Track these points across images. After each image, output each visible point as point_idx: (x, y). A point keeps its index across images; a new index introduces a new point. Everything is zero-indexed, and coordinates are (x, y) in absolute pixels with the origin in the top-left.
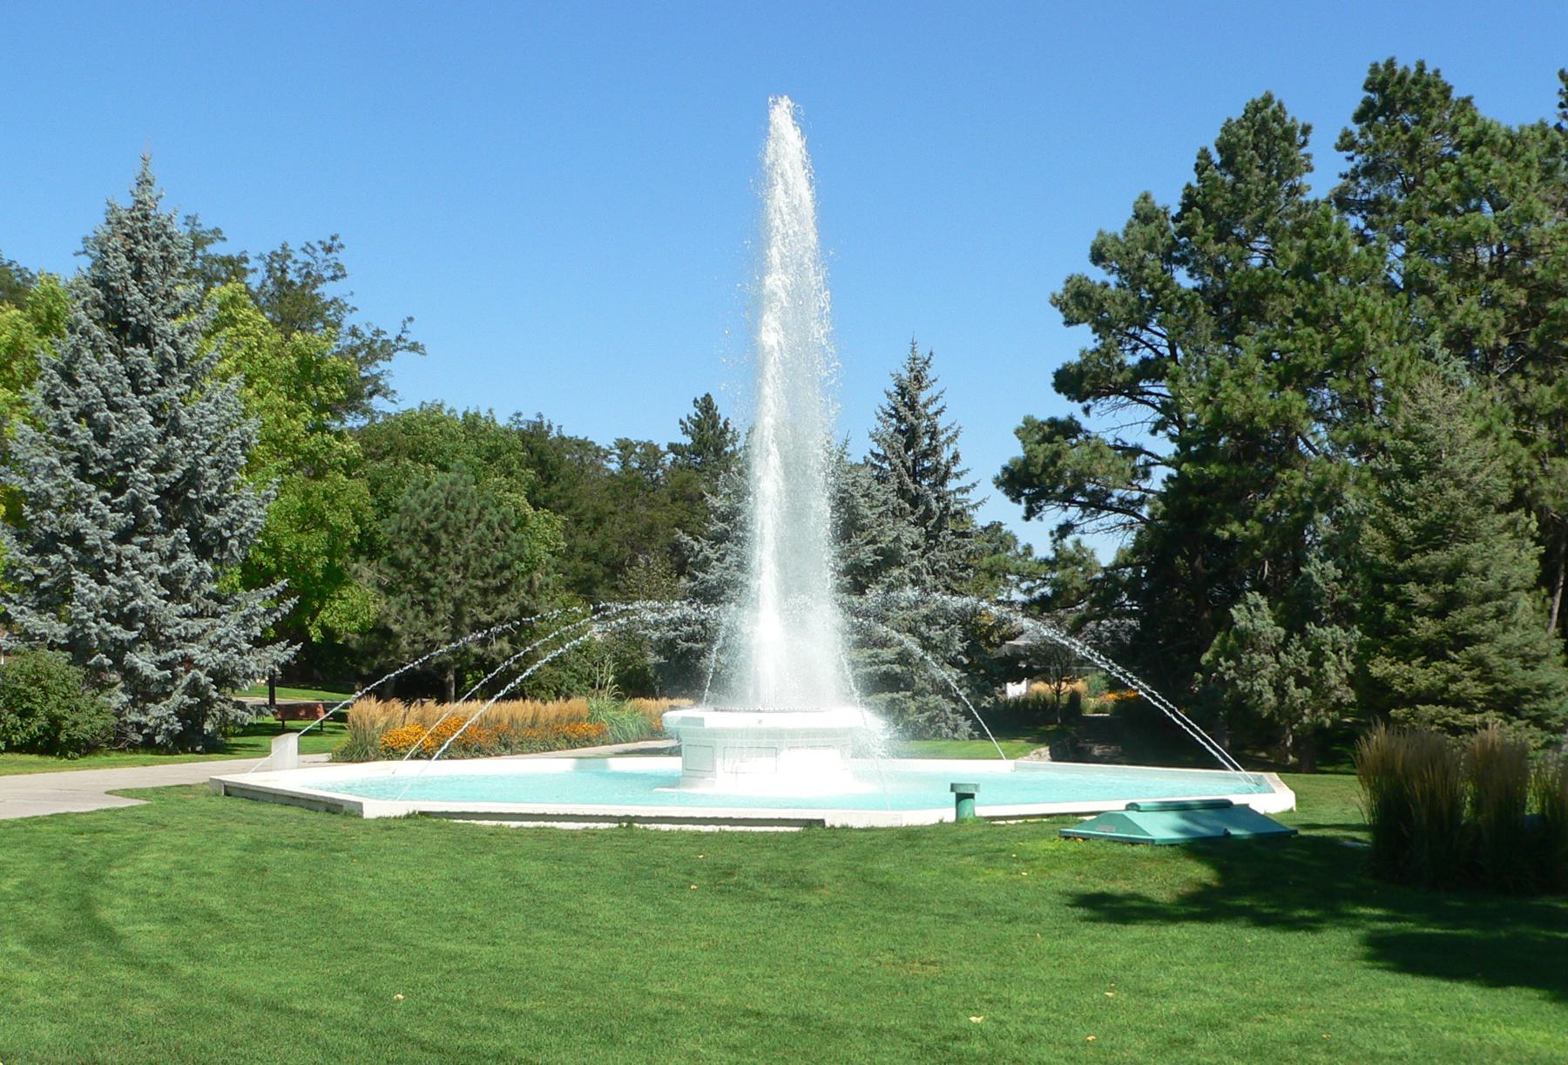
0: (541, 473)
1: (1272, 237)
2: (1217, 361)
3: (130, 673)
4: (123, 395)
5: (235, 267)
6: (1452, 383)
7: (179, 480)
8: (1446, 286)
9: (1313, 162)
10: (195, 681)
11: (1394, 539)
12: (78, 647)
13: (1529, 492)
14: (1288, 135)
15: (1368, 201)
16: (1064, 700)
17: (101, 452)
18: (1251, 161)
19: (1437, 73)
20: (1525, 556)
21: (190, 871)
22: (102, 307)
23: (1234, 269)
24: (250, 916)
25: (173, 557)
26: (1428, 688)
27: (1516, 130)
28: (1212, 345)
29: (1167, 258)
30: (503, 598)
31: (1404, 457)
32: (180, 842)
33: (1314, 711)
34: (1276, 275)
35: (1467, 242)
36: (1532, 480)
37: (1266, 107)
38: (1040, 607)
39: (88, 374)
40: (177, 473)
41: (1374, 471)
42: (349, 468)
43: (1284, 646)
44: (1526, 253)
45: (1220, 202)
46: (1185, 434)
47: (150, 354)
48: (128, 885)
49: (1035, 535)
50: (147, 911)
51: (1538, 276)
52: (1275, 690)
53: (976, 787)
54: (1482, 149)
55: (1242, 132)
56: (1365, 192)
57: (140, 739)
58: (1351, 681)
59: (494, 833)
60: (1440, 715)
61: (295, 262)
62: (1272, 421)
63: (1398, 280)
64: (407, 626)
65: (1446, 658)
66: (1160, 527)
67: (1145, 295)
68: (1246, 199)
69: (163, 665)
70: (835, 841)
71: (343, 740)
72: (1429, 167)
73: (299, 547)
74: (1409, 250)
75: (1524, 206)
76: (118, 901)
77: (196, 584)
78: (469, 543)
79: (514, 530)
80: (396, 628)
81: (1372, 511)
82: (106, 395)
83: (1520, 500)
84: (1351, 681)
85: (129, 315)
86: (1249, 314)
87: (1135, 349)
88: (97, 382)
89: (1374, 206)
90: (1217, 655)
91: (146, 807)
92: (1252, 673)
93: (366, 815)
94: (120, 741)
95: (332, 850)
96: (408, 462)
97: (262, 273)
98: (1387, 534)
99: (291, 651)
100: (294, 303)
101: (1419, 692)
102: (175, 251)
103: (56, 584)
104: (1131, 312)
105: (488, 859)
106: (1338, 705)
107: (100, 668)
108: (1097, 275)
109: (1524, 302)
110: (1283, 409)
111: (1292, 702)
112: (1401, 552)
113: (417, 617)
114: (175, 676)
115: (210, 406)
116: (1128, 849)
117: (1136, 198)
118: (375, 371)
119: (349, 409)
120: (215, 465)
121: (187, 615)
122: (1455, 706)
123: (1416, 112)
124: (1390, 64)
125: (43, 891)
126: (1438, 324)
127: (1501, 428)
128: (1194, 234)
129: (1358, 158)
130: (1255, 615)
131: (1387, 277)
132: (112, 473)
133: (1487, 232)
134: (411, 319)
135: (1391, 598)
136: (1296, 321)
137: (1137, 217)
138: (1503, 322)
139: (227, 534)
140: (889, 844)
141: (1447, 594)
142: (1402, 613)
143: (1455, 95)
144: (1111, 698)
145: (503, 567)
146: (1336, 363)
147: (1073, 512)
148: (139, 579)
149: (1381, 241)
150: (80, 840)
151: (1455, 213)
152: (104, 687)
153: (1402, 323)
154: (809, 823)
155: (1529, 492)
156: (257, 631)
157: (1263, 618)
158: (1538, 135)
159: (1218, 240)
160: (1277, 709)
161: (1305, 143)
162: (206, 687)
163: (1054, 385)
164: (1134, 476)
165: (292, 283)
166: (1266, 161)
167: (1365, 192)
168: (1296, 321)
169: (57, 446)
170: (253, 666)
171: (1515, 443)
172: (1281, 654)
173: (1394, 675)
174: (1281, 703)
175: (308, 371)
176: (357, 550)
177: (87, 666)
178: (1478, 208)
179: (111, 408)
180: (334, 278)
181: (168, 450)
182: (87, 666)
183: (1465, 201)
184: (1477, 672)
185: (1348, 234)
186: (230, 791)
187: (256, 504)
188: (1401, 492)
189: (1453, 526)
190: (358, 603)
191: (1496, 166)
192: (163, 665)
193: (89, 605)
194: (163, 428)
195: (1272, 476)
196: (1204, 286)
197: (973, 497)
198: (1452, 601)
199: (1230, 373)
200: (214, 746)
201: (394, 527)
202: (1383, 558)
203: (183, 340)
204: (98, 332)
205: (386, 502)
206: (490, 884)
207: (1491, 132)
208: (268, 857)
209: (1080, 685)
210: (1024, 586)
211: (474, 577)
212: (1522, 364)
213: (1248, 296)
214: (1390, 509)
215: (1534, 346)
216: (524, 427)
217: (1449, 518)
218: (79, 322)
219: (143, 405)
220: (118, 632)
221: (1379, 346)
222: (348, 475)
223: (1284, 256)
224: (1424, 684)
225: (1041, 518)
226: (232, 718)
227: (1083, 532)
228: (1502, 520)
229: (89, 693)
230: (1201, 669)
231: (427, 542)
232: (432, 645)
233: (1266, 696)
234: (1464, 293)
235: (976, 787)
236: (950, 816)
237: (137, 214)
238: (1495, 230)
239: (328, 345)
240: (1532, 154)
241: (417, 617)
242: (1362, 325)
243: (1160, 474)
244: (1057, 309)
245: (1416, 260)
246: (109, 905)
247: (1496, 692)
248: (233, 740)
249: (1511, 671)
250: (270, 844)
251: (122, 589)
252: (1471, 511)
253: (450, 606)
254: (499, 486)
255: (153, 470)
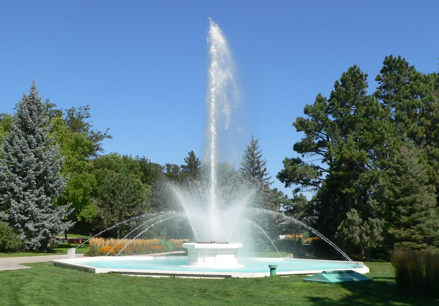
0: (144, 173)
1: (357, 106)
2: (341, 142)
3: (26, 229)
4: (26, 149)
5: (59, 113)
6: (410, 148)
7: (42, 174)
8: (408, 120)
9: (368, 85)
10: (45, 232)
11: (394, 193)
12: (11, 221)
13: (433, 179)
14: (361, 77)
15: (385, 95)
16: (297, 240)
17: (19, 165)
18: (350, 84)
19: (404, 59)
20: (432, 198)
21: (46, 288)
22: (21, 124)
23: (346, 115)
24: (65, 303)
25: (39, 196)
26: (405, 237)
27: (427, 75)
28: (339, 137)
29: (326, 112)
30: (134, 209)
31: (397, 169)
32: (43, 279)
33: (371, 243)
34: (358, 117)
35: (414, 107)
36: (434, 176)
37: (355, 69)
38: (289, 212)
39: (17, 143)
40: (41, 171)
41: (388, 173)
42: (90, 170)
43: (362, 224)
44: (430, 110)
45: (342, 96)
46: (332, 163)
47: (34, 137)
48: (28, 292)
49: (288, 192)
50: (34, 301)
51: (434, 116)
52: (360, 237)
53: (276, 266)
54: (418, 80)
55: (348, 76)
56: (384, 93)
57: (29, 248)
58: (382, 234)
59: (134, 278)
60: (409, 245)
61: (76, 112)
62: (357, 159)
63: (394, 118)
64: (106, 217)
65: (410, 228)
66: (325, 190)
67: (320, 122)
68: (349, 95)
69: (36, 227)
70: (235, 282)
71: (88, 249)
72: (402, 86)
73: (75, 193)
74: (396, 110)
75: (430, 96)
76: (25, 297)
77: (46, 204)
78: (124, 193)
79: (137, 189)
80: (103, 217)
81: (387, 185)
82: (21, 149)
83: (431, 182)
84: (382, 234)
85: (28, 126)
86: (350, 128)
87: (317, 138)
88: (19, 145)
89: (386, 97)
90: (342, 227)
91: (32, 269)
92: (353, 232)
93: (96, 273)
94: (23, 249)
95: (87, 283)
96: (107, 170)
97: (67, 115)
98: (392, 192)
99: (73, 224)
100: (76, 124)
101: (403, 238)
102: (42, 108)
103: (5, 203)
104: (316, 128)
105: (133, 286)
106: (378, 242)
107: (18, 227)
108: (306, 117)
109: (430, 124)
110: (361, 155)
111: (364, 240)
112: (397, 197)
113: (109, 214)
114: (39, 230)
115: (51, 152)
116: (323, 285)
117: (317, 95)
118: (98, 143)
119: (90, 154)
120: (52, 169)
121: (43, 213)
122: (414, 242)
123: (398, 70)
124: (391, 57)
125: (3, 294)
126: (406, 131)
127: (424, 160)
128: (334, 105)
129: (382, 83)
130: (353, 215)
131: (390, 117)
132: (22, 171)
133: (419, 104)
134: (109, 129)
135: (394, 210)
136: (365, 130)
137: (317, 100)
138: (424, 130)
139: (55, 189)
140: (252, 283)
141: (410, 209)
142: (397, 215)
143: (409, 66)
144: (310, 240)
145: (134, 200)
146: (376, 142)
147: (299, 185)
148: (30, 202)
149: (388, 107)
150: (13, 278)
151: (410, 99)
152: (19, 233)
153: (395, 130)
154: (227, 276)
155: (433, 179)
156: (63, 218)
157: (356, 216)
158: (433, 76)
159: (341, 107)
160: (360, 242)
161: (366, 79)
162: (48, 234)
163: (293, 149)
164: (318, 175)
165: (75, 118)
166: (355, 84)
167: (384, 93)
168: (365, 130)
169: (7, 163)
170: (62, 228)
171: (428, 165)
172: (361, 227)
173: (395, 233)
174: (361, 241)
175: (78, 143)
176: (92, 195)
177: (14, 227)
178: (417, 97)
179: (22, 152)
180: (87, 117)
181: (39, 165)
182: (14, 227)
183: (413, 95)
184: (420, 232)
185: (379, 105)
186: (56, 264)
187: (63, 181)
188: (396, 179)
189: (412, 189)
190: (91, 210)
191: (421, 85)
192: (36, 227)
193: (15, 209)
194: (37, 158)
195: (358, 175)
196: (337, 120)
197: (270, 181)
198: (412, 211)
199: (345, 145)
200: (50, 251)
201: (103, 188)
202: (391, 199)
203: (44, 133)
204: (19, 131)
205: (100, 181)
206: (135, 294)
207: (420, 75)
208: (69, 284)
209: (301, 236)
210: (285, 207)
211: (126, 203)
212: (430, 142)
213: (350, 123)
214: (393, 184)
215: (433, 137)
216: (140, 160)
217: (411, 187)
218: (14, 128)
219: (32, 152)
220: (23, 217)
221: (388, 137)
222: (89, 173)
223: (361, 111)
224: (404, 235)
225: (290, 187)
226: (55, 243)
227: (302, 191)
228: (426, 187)
229: (14, 235)
230: (337, 231)
231: (112, 193)
232: (113, 223)
233: (357, 239)
234: (413, 122)
235: (276, 266)
236: (268, 274)
237: (31, 97)
238: (422, 103)
239: (84, 137)
240: (432, 82)
241: (109, 214)
242: (384, 131)
243: (325, 174)
244: (294, 127)
245: (399, 112)
246: (23, 298)
247: (425, 238)
248: (55, 249)
249: (430, 232)
250: (69, 281)
251: (25, 205)
252: (417, 185)
253: (118, 211)
254: (133, 177)
255: (34, 170)
